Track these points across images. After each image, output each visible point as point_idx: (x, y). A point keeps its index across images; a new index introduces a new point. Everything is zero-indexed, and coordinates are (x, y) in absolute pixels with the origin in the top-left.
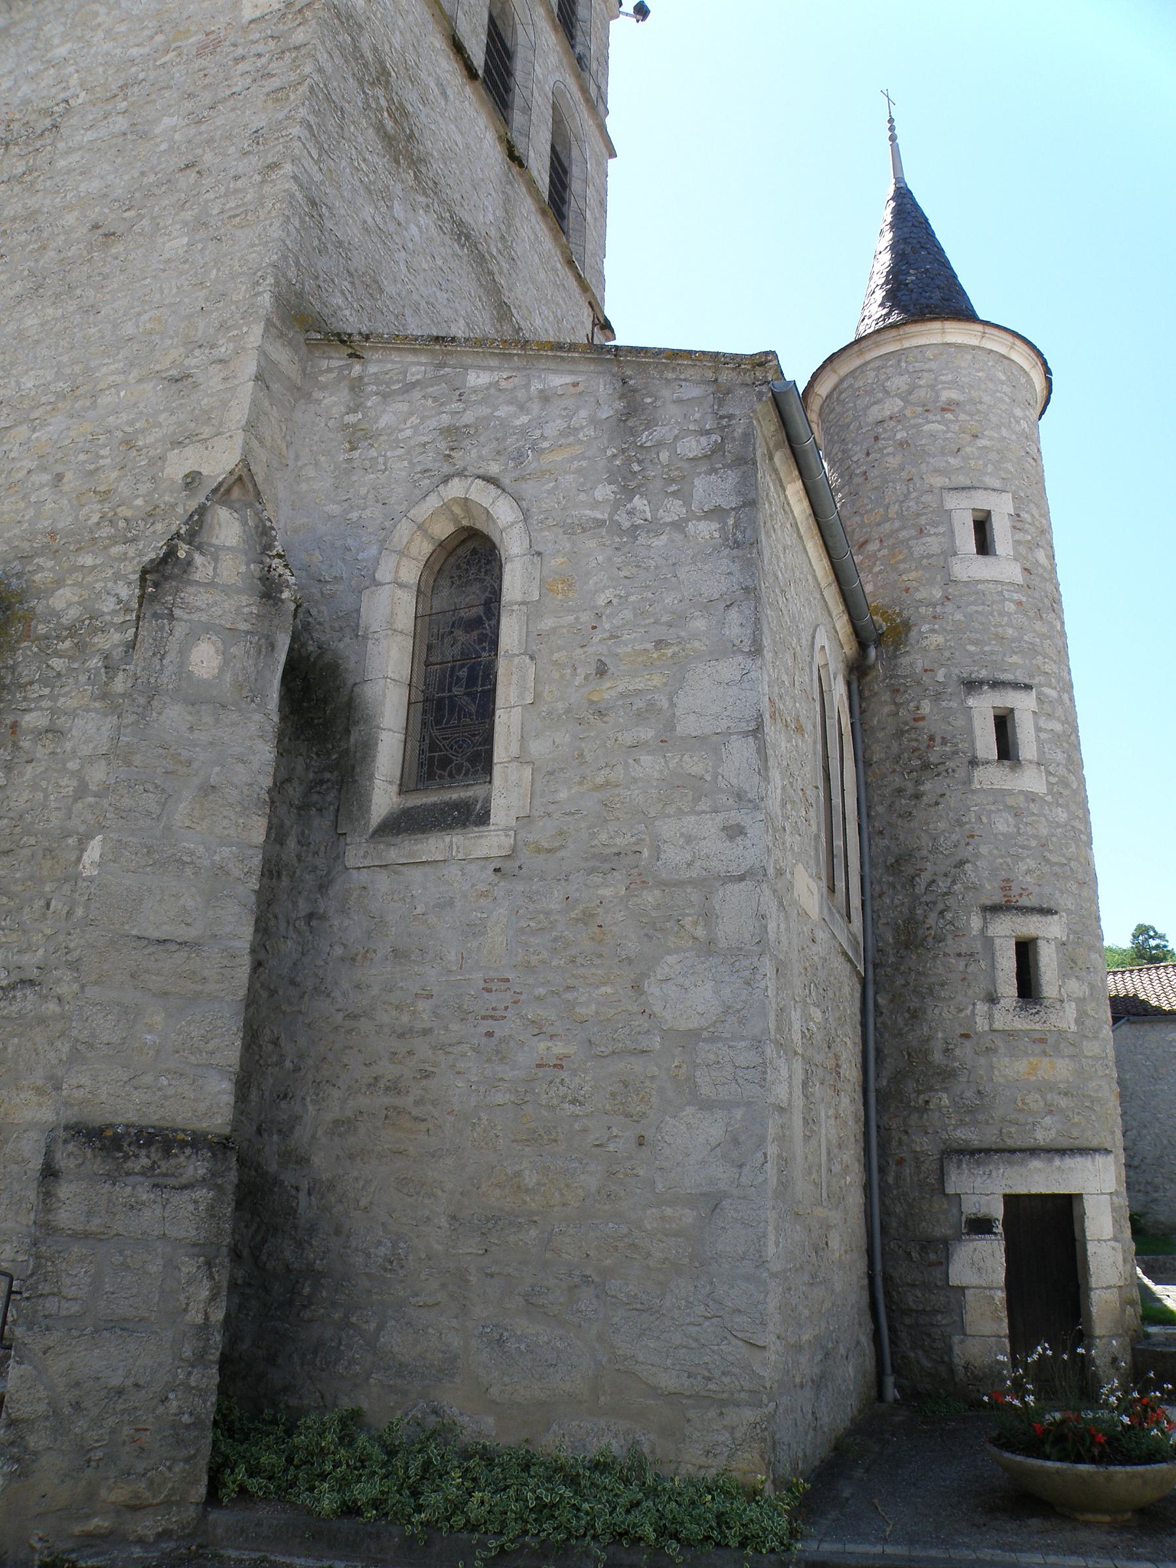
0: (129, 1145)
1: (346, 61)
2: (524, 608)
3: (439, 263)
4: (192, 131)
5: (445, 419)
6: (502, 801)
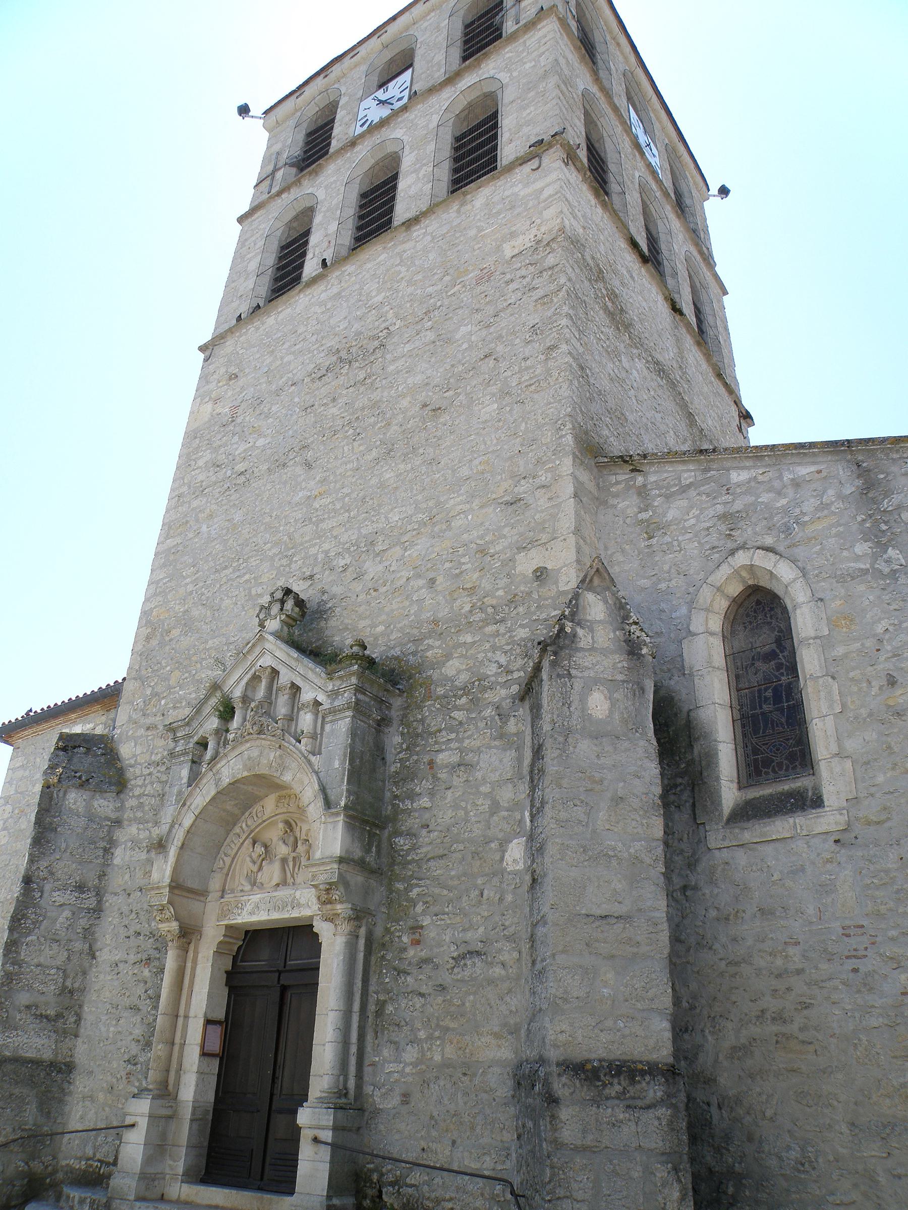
0: (605, 1076)
1: (581, 270)
2: (818, 641)
3: (652, 393)
4: (484, 333)
5: (720, 509)
6: (831, 788)
